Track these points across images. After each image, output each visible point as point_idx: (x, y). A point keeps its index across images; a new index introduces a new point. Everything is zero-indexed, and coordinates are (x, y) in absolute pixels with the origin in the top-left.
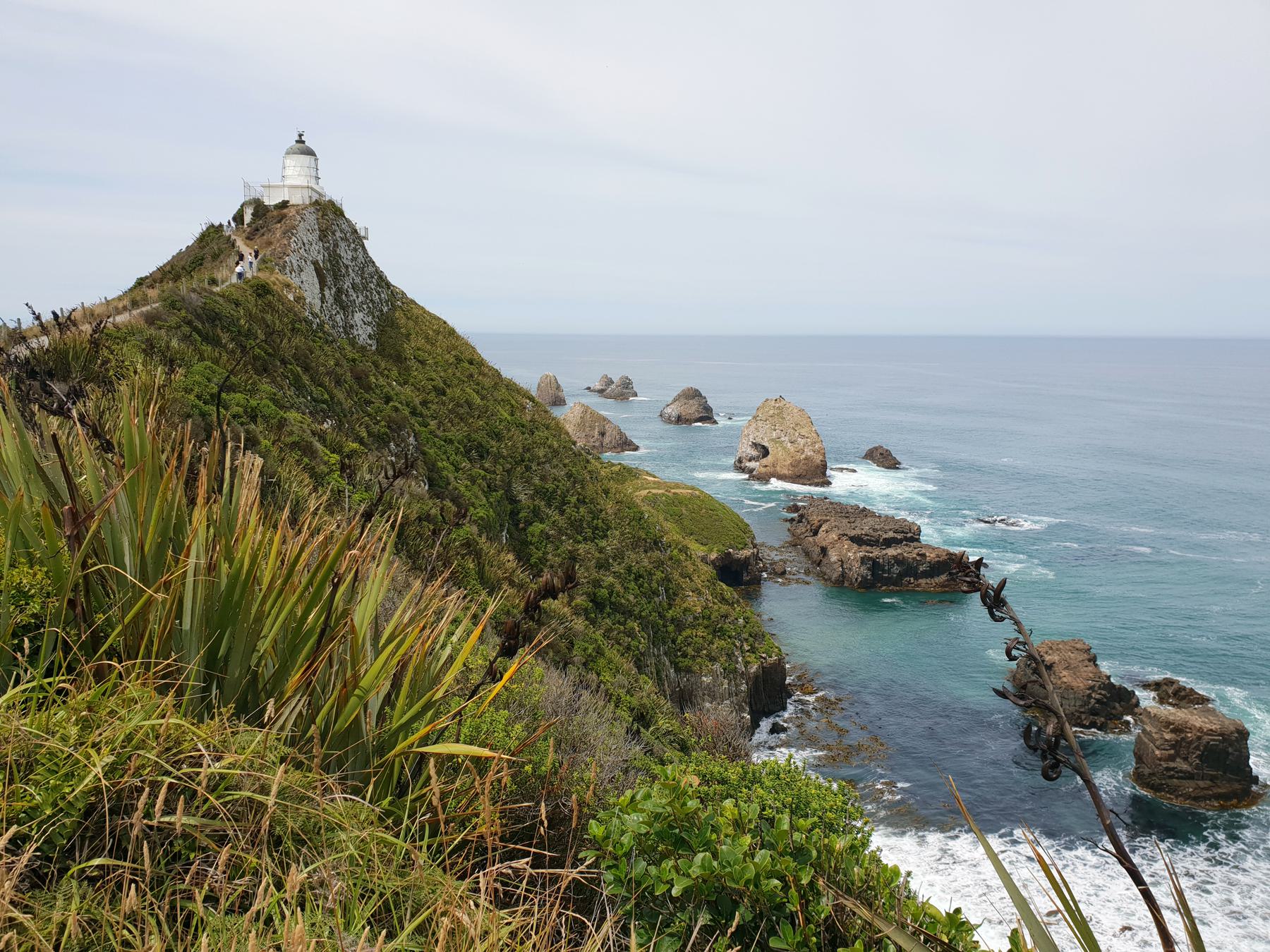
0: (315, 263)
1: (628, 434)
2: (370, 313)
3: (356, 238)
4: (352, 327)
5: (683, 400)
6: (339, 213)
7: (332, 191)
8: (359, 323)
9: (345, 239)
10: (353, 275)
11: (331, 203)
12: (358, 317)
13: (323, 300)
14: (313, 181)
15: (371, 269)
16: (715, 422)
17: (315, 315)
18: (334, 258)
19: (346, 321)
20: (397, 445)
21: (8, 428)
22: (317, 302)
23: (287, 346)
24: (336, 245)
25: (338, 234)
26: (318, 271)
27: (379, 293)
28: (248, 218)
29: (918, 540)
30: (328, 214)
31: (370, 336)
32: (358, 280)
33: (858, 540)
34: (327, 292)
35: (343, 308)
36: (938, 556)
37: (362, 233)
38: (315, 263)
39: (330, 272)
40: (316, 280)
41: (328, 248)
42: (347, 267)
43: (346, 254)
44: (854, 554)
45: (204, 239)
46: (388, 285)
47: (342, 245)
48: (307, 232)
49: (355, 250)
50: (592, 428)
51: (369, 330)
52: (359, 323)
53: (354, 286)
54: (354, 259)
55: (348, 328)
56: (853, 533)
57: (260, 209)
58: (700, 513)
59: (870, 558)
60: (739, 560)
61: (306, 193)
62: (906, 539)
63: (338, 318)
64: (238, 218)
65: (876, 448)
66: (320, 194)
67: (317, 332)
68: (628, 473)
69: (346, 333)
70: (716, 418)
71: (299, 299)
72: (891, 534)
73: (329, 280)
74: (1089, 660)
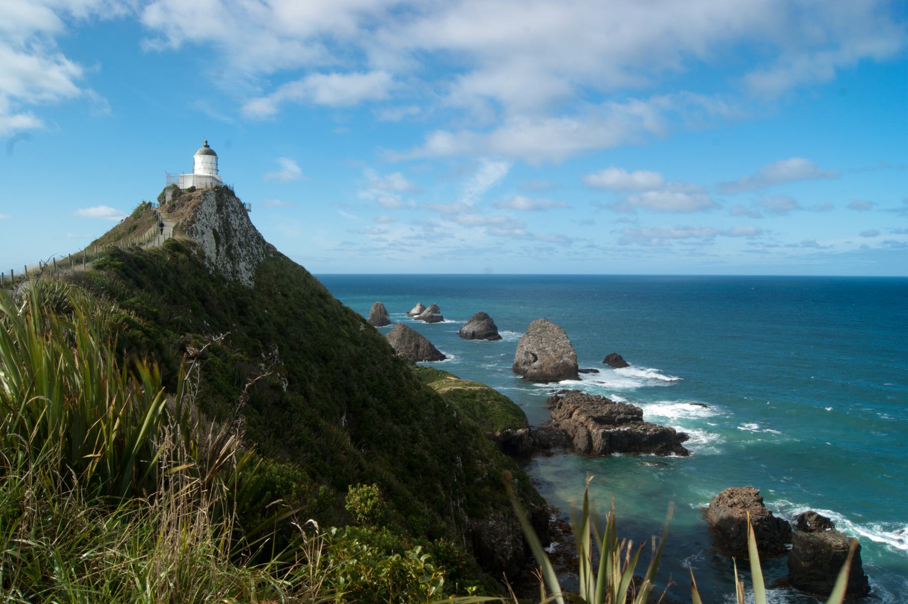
0: (214, 230)
1: (436, 347)
2: (251, 262)
3: (242, 210)
4: (237, 272)
5: (476, 322)
6: (231, 193)
7: (227, 180)
8: (243, 269)
9: (234, 212)
10: (239, 236)
11: (226, 187)
12: (242, 265)
13: (218, 253)
14: (214, 172)
15: (252, 232)
16: (500, 338)
17: (211, 264)
18: (226, 223)
19: (233, 268)
20: (267, 355)
21: (547, 19)
22: (214, 256)
23: (196, 302)
24: (228, 216)
25: (230, 209)
26: (215, 233)
27: (257, 248)
28: (169, 198)
29: (641, 420)
30: (223, 195)
31: (250, 279)
32: (243, 239)
33: (600, 421)
34: (221, 249)
35: (232, 259)
36: (655, 431)
37: (247, 207)
38: (214, 230)
39: (223, 235)
40: (213, 240)
41: (222, 218)
42: (235, 231)
43: (235, 223)
44: (597, 432)
45: (137, 215)
46: (264, 242)
47: (233, 216)
48: (210, 208)
49: (242, 219)
50: (410, 342)
51: (250, 274)
52: (243, 269)
53: (240, 244)
54: (241, 225)
55: (235, 272)
56: (596, 415)
57: (177, 192)
58: (480, 402)
59: (607, 433)
60: (516, 437)
61: (209, 181)
62: (633, 419)
63: (228, 266)
64: (162, 198)
65: (612, 355)
66: (218, 181)
67: (218, 279)
68: (440, 374)
69: (233, 276)
70: (500, 333)
71: (202, 254)
72: (622, 416)
73: (223, 240)
74: (758, 501)
